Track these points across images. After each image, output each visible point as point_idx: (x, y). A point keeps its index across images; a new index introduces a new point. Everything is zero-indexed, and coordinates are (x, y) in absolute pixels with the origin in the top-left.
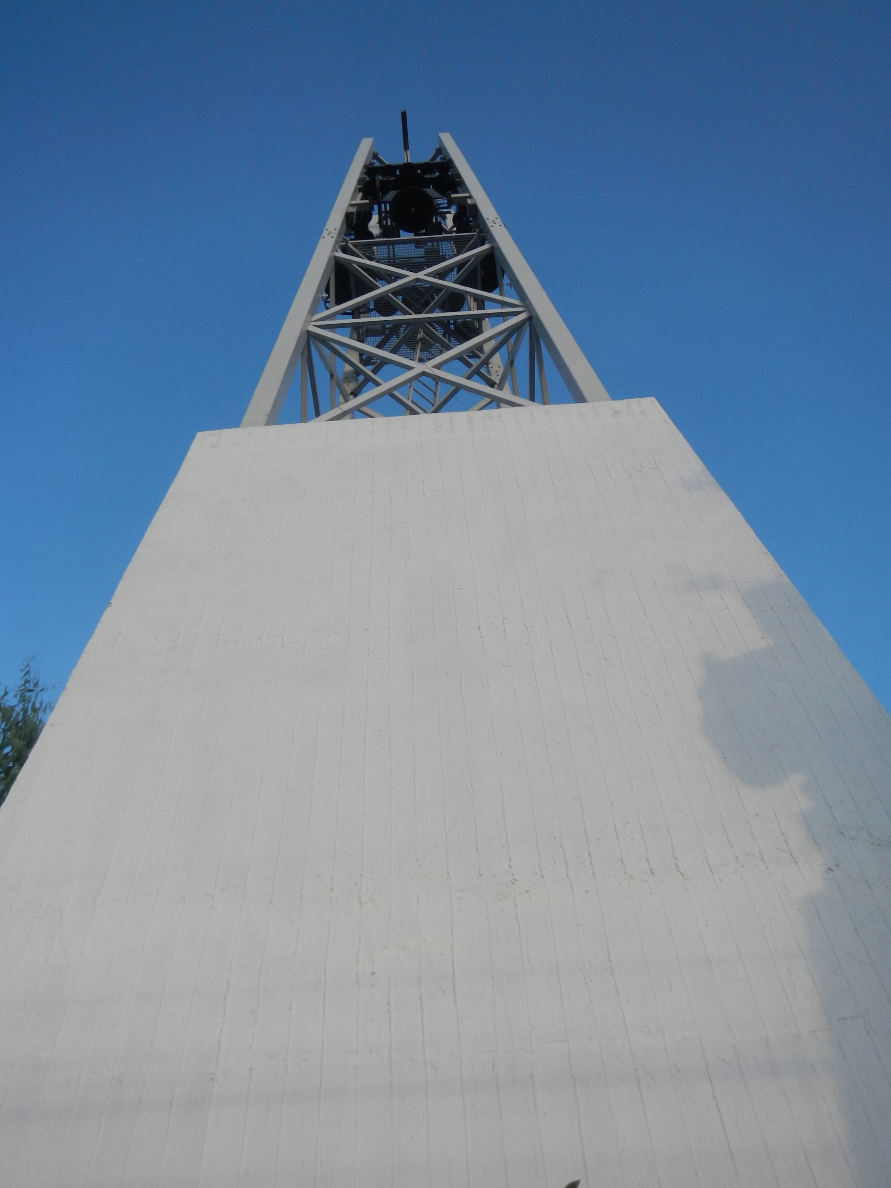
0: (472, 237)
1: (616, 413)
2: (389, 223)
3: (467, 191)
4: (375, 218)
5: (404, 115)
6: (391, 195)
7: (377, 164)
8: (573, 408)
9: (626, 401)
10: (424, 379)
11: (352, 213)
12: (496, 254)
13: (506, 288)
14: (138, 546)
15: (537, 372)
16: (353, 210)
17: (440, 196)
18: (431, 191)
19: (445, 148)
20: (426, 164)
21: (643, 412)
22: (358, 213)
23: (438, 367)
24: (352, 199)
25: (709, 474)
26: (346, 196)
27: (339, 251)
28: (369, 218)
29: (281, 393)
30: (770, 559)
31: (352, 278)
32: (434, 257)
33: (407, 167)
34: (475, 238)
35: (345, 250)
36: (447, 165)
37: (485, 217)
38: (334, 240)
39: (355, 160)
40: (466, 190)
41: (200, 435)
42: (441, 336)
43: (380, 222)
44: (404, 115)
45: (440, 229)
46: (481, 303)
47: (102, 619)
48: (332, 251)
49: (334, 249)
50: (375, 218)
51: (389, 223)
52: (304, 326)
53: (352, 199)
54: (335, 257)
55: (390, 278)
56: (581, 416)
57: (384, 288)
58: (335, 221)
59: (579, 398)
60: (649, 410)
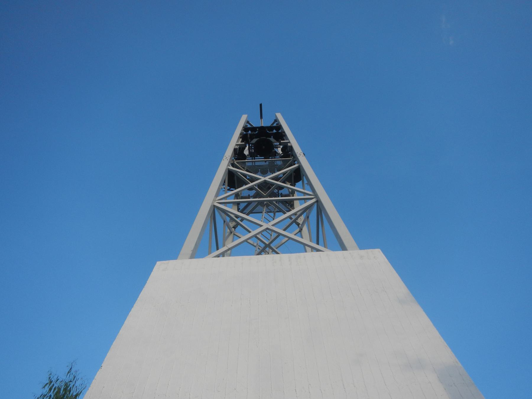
0: (290, 160)
1: (362, 257)
3: (288, 139)
4: (247, 148)
5: (261, 105)
6: (254, 141)
7: (249, 126)
8: (341, 253)
9: (366, 251)
11: (237, 149)
13: (306, 186)
14: (120, 329)
15: (323, 235)
16: (237, 147)
18: (272, 139)
20: (270, 127)
22: (240, 148)
23: (273, 225)
24: (237, 142)
25: (411, 294)
26: (235, 141)
29: (200, 238)
30: (449, 350)
31: (235, 178)
33: (262, 128)
35: (233, 165)
36: (279, 127)
39: (241, 121)
40: (288, 139)
41: (158, 263)
43: (249, 149)
44: (261, 105)
45: (276, 154)
46: (293, 192)
47: (96, 377)
49: (228, 165)
50: (247, 148)
53: (237, 142)
55: (252, 180)
56: (344, 258)
57: (251, 184)
60: (376, 258)
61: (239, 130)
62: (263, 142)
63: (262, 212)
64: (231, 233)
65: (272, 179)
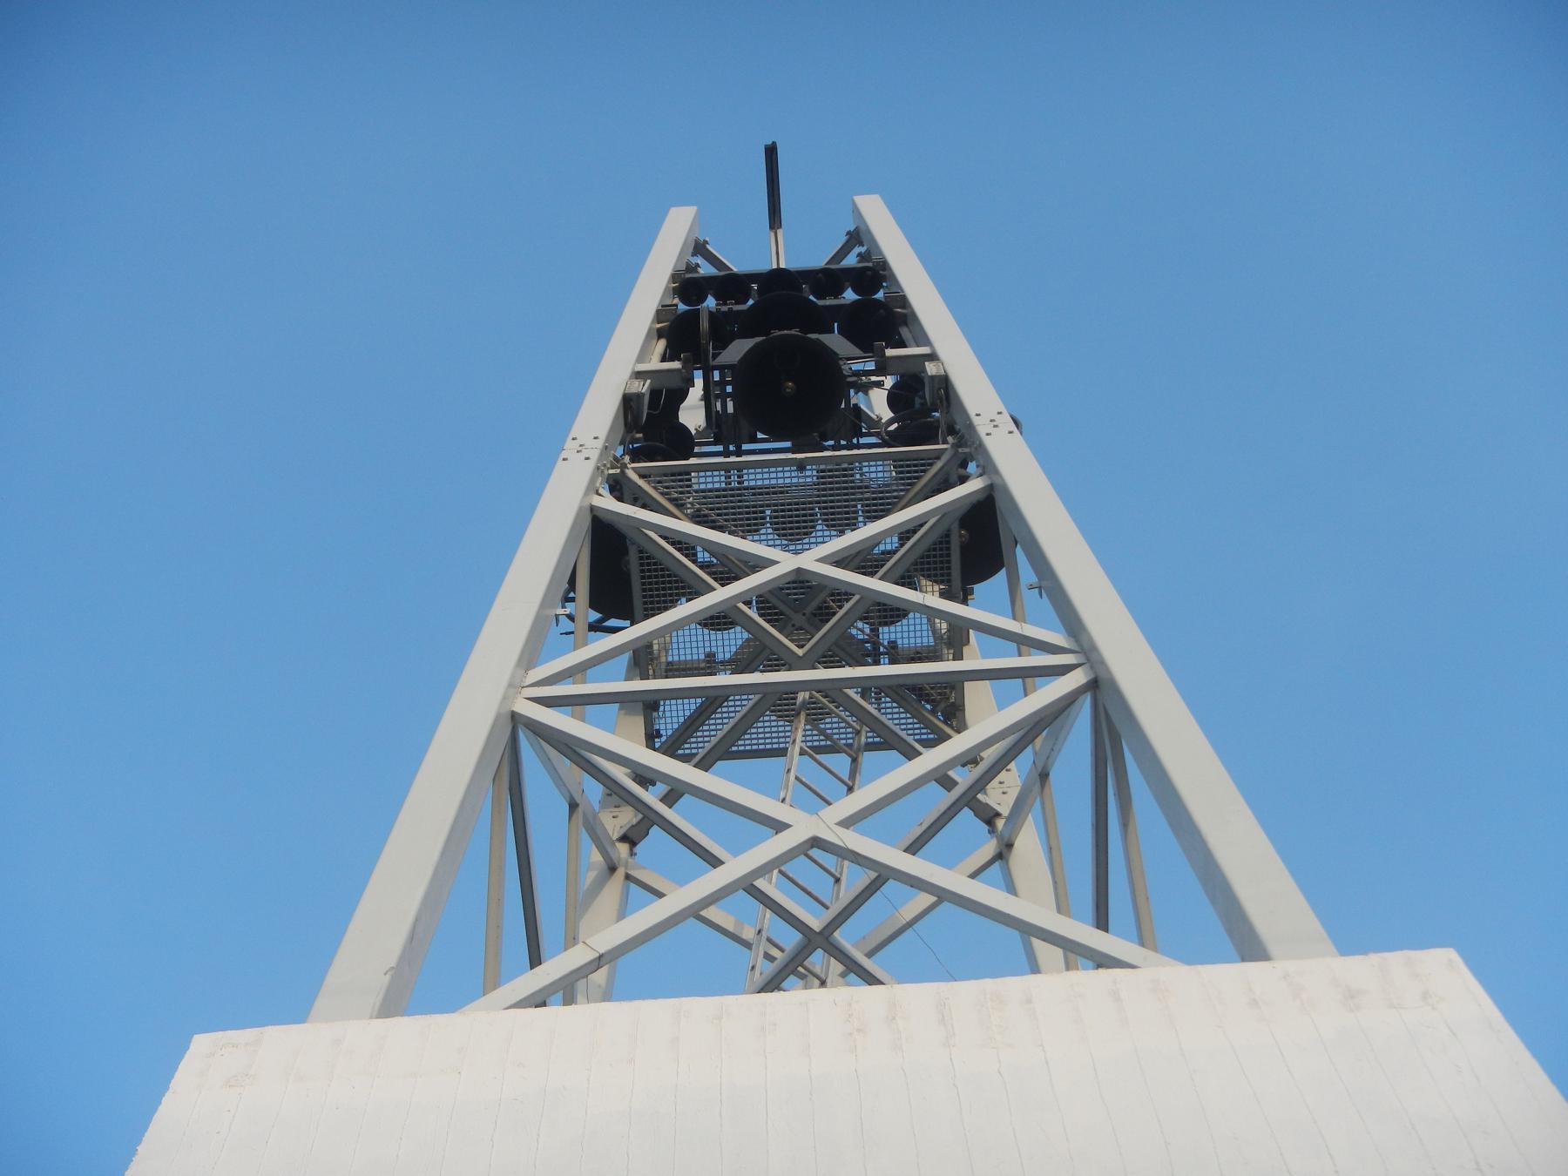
0: (938, 455)
2: (730, 409)
4: (696, 392)
5: (771, 152)
6: (737, 350)
7: (706, 269)
8: (1231, 976)
9: (1374, 959)
10: (815, 853)
11: (639, 396)
12: (1000, 503)
13: (1029, 597)
15: (1132, 880)
16: (643, 387)
17: (857, 352)
18: (835, 341)
19: (869, 232)
20: (824, 271)
21: (1425, 996)
22: (655, 393)
23: (847, 823)
26: (627, 353)
27: (605, 491)
28: (683, 395)
31: (633, 557)
32: (840, 504)
33: (778, 280)
34: (945, 458)
35: (618, 488)
36: (874, 274)
37: (972, 411)
38: (589, 467)
41: (201, 1043)
42: (858, 698)
43: (707, 397)
44: (771, 152)
45: (857, 422)
48: (586, 493)
50: (696, 392)
51: (730, 409)
52: (505, 698)
54: (592, 508)
55: (728, 568)
57: (720, 595)
58: (597, 417)
59: (1249, 947)
61: (649, 292)
62: (786, 356)
63: (782, 752)
64: (612, 869)
65: (840, 561)
